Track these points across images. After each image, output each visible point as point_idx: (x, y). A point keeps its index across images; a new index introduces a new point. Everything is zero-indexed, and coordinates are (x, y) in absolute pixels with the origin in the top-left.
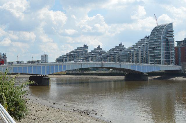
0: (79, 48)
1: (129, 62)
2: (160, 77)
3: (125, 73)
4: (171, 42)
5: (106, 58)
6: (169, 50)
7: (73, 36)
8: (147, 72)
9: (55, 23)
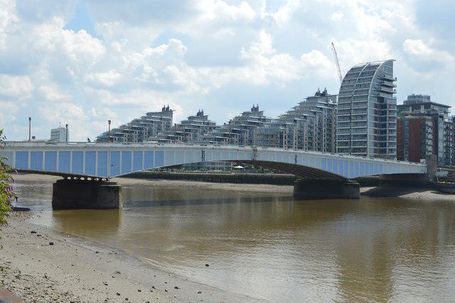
0: (153, 113)
1: (281, 147)
2: (371, 190)
3: (295, 179)
4: (390, 105)
5: (234, 135)
6: (385, 124)
7: (117, 89)
8: (354, 177)
9: (73, 56)
